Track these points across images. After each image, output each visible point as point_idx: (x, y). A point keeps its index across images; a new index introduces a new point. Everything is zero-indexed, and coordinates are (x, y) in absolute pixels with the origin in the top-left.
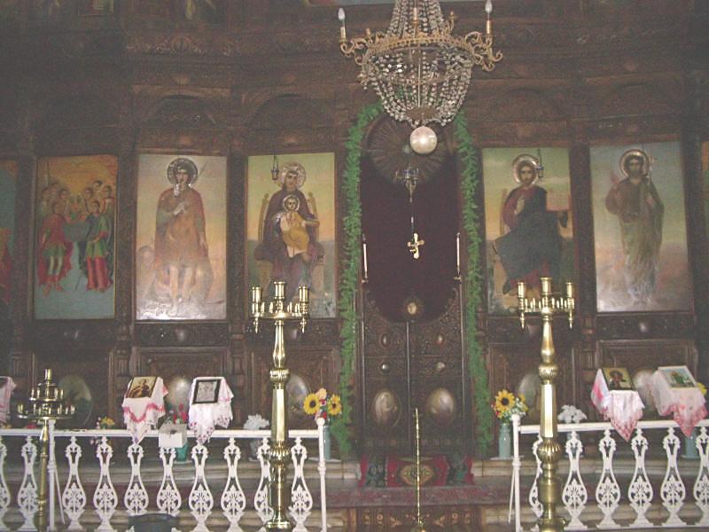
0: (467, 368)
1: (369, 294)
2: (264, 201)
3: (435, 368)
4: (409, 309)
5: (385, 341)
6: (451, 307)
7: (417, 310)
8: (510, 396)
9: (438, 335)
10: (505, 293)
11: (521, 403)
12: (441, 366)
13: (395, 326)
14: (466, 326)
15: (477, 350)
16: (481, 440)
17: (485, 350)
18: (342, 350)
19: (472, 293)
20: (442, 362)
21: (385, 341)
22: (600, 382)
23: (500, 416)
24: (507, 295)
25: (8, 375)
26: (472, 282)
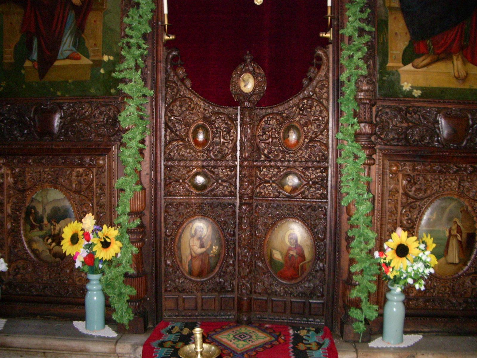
0: (337, 188)
1: (175, 58)
2: (367, 355)
3: (282, 186)
4: (242, 85)
5: (201, 137)
6: (314, 83)
7: (257, 85)
8: (412, 243)
9: (288, 130)
10: (405, 63)
11: (428, 253)
12: (293, 181)
13: (219, 113)
14: (338, 113)
15: (356, 157)
16: (354, 313)
17: (369, 157)
18: (122, 149)
19: (351, 57)
20: (296, 174)
21: (201, 137)
22: (58, 122)
23: (391, 275)
24: (409, 67)
25: (438, 147)
26: (350, 38)
